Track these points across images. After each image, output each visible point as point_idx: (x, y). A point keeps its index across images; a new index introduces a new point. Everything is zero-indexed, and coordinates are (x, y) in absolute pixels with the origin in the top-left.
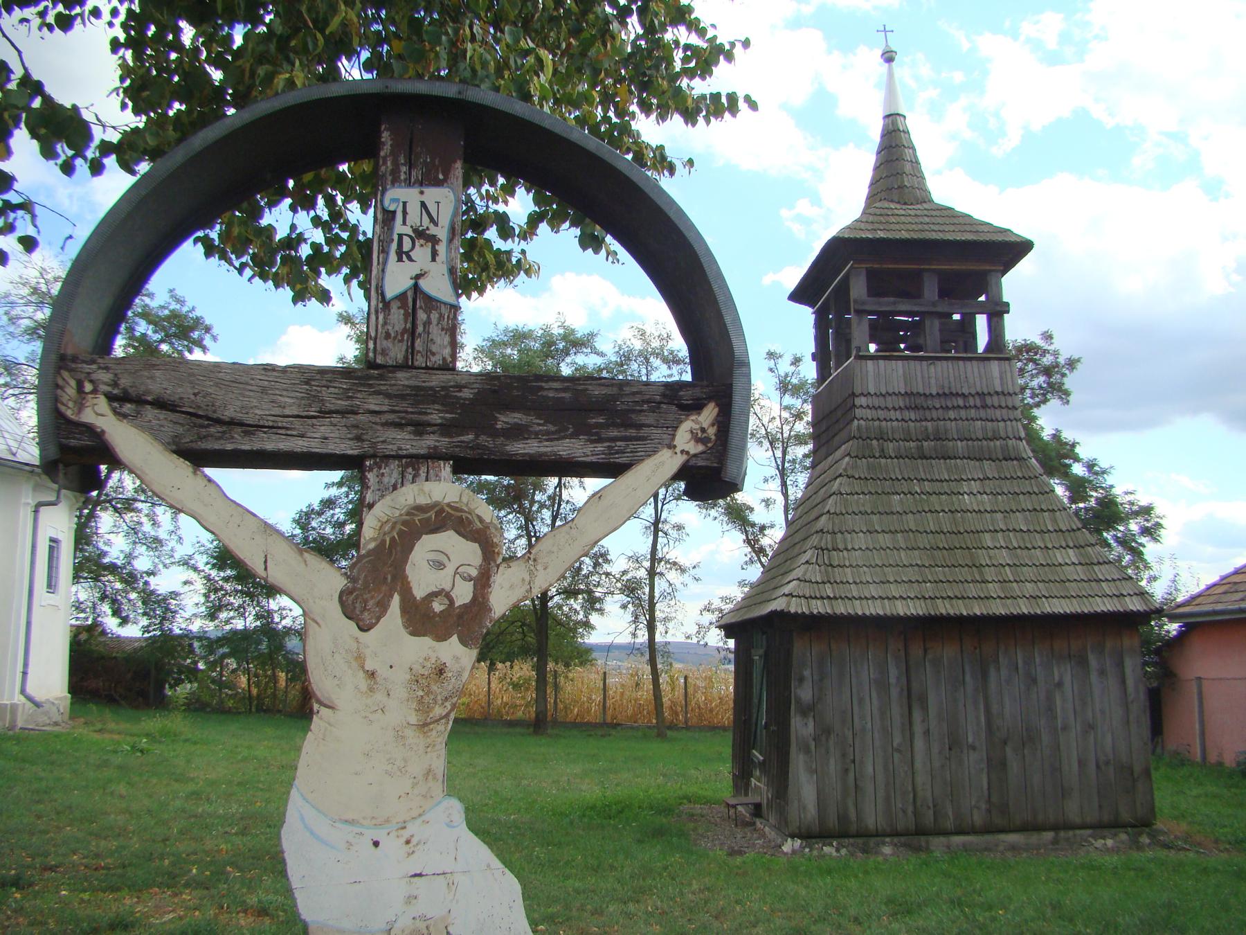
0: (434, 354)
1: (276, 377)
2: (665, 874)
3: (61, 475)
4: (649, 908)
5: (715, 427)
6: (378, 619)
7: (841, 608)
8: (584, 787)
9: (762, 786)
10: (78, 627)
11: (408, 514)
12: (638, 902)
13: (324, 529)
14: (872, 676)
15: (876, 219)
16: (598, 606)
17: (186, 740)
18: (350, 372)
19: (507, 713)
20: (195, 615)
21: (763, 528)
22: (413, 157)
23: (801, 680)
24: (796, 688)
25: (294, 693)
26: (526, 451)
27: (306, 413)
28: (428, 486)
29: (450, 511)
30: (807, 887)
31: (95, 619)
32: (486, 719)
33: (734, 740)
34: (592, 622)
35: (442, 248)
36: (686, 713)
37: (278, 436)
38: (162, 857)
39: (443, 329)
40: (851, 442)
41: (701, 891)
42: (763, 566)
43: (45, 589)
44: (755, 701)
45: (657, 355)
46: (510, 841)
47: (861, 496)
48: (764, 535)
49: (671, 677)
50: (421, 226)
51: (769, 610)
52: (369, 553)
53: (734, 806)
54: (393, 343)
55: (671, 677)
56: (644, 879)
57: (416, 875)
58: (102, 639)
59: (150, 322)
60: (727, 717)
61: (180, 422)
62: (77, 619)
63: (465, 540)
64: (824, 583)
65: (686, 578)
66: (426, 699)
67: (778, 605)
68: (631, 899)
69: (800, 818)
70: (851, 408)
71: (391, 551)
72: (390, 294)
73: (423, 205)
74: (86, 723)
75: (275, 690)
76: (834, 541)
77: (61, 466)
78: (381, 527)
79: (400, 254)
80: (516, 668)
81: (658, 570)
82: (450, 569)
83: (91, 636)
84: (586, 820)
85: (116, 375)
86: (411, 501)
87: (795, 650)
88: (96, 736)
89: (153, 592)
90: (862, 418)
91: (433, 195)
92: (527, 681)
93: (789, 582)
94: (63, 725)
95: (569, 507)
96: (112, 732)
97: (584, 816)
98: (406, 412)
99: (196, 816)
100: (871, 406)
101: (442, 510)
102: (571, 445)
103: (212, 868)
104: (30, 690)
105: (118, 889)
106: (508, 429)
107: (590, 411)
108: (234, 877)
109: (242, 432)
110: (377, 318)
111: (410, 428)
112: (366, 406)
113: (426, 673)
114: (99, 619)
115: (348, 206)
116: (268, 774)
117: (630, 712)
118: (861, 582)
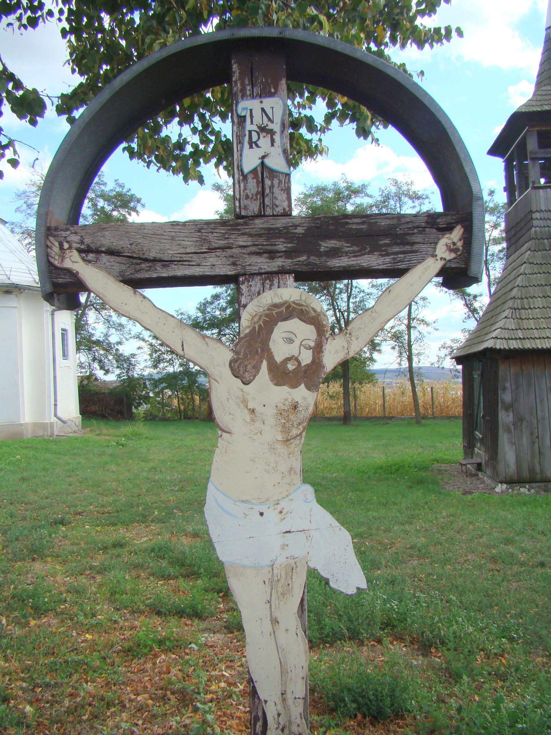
0: (277, 206)
1: (180, 229)
2: (426, 507)
3: (56, 300)
4: (418, 527)
5: (462, 241)
6: (254, 377)
7: (528, 345)
8: (375, 455)
9: (482, 453)
10: (82, 377)
11: (268, 310)
12: (411, 523)
13: (215, 312)
14: (548, 385)
15: (542, 98)
16: (377, 348)
17: (147, 438)
18: (225, 222)
19: (327, 413)
20: (146, 367)
21: (475, 297)
22: (254, 79)
23: (504, 389)
24: (501, 394)
25: (205, 407)
26: (340, 265)
27: (200, 251)
28: (280, 291)
29: (295, 306)
30: (512, 513)
31: (91, 372)
32: (315, 417)
33: (463, 423)
34: (374, 358)
35: (277, 137)
36: (433, 409)
37: (184, 266)
38: (138, 505)
39: (282, 190)
40: (531, 242)
41: (448, 516)
42: (476, 320)
43: (62, 358)
44: (476, 402)
45: (406, 195)
46: (334, 489)
47: (538, 275)
48: (476, 301)
49: (423, 388)
50: (263, 124)
51: (484, 348)
52: (246, 336)
53: (465, 465)
54: (251, 202)
55: (423, 388)
56: (414, 510)
57: (287, 532)
58: (96, 383)
59: (105, 200)
60: (459, 410)
61: (124, 262)
62: (81, 372)
63: (305, 324)
64: (516, 329)
65: (429, 329)
66: (287, 425)
67: (489, 344)
68: (406, 522)
69: (505, 471)
70: (530, 220)
71: (260, 334)
72: (246, 170)
73: (263, 110)
74: (91, 431)
75: (194, 406)
76: (522, 303)
77: (55, 295)
78: (252, 319)
79: (251, 144)
80: (331, 386)
81: (413, 325)
82: (297, 343)
83: (89, 381)
84: (377, 475)
85: (82, 236)
86: (269, 301)
87: (500, 372)
88: (96, 438)
89: (121, 355)
90: (537, 226)
91: (269, 103)
92: (338, 393)
93: (495, 330)
94: (79, 432)
95: (357, 290)
96: (105, 435)
97: (376, 473)
98: (263, 245)
99: (154, 481)
100: (543, 218)
101: (289, 306)
102: (369, 259)
103: (166, 511)
104: (59, 414)
105: (116, 524)
106: (328, 251)
107: (380, 236)
108: (179, 515)
109: (162, 265)
110: (240, 186)
111: (266, 255)
112: (237, 243)
113: (286, 408)
114: (93, 372)
115: (213, 119)
116: (193, 455)
117: (399, 410)
118: (540, 328)
